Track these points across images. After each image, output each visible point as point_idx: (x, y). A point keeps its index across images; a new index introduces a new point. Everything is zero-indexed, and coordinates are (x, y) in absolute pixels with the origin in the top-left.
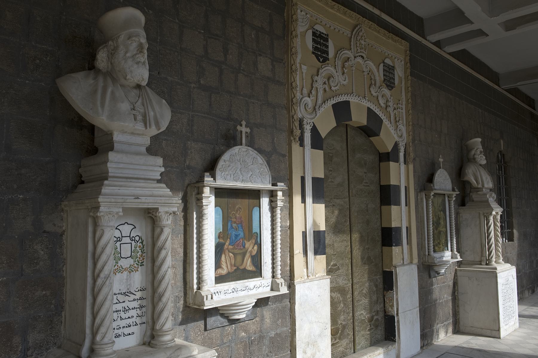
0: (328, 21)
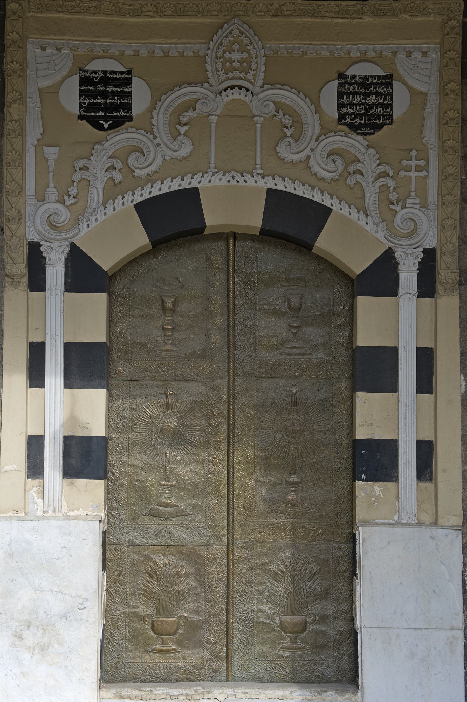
0: (129, 43)
